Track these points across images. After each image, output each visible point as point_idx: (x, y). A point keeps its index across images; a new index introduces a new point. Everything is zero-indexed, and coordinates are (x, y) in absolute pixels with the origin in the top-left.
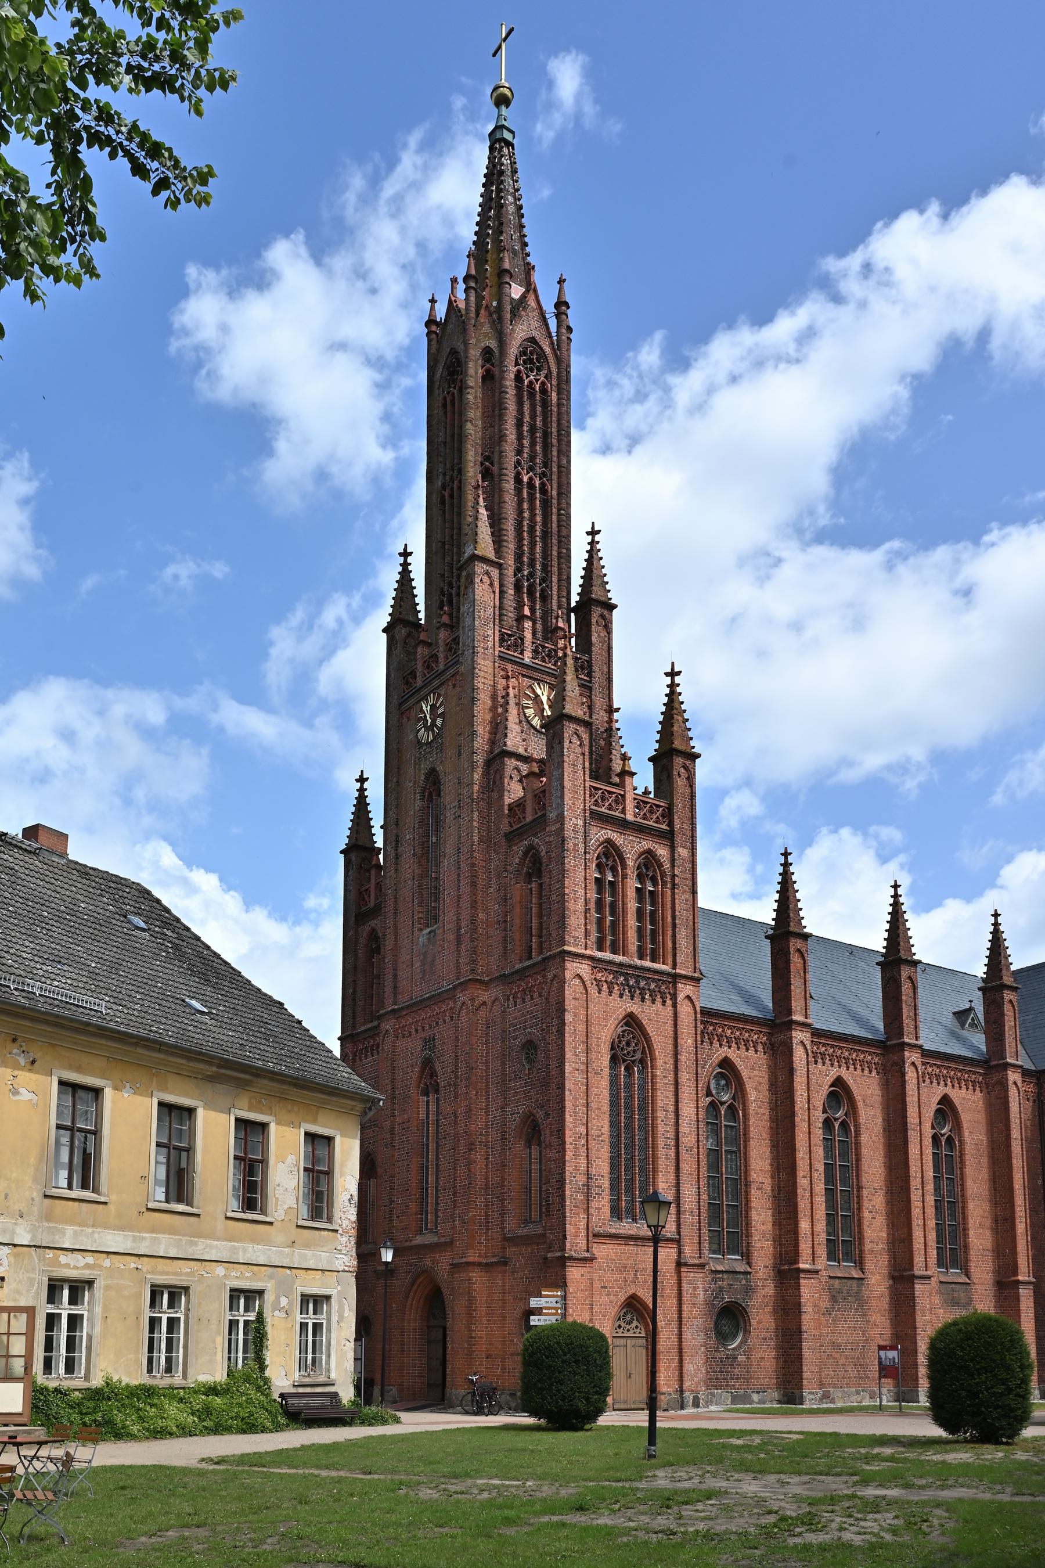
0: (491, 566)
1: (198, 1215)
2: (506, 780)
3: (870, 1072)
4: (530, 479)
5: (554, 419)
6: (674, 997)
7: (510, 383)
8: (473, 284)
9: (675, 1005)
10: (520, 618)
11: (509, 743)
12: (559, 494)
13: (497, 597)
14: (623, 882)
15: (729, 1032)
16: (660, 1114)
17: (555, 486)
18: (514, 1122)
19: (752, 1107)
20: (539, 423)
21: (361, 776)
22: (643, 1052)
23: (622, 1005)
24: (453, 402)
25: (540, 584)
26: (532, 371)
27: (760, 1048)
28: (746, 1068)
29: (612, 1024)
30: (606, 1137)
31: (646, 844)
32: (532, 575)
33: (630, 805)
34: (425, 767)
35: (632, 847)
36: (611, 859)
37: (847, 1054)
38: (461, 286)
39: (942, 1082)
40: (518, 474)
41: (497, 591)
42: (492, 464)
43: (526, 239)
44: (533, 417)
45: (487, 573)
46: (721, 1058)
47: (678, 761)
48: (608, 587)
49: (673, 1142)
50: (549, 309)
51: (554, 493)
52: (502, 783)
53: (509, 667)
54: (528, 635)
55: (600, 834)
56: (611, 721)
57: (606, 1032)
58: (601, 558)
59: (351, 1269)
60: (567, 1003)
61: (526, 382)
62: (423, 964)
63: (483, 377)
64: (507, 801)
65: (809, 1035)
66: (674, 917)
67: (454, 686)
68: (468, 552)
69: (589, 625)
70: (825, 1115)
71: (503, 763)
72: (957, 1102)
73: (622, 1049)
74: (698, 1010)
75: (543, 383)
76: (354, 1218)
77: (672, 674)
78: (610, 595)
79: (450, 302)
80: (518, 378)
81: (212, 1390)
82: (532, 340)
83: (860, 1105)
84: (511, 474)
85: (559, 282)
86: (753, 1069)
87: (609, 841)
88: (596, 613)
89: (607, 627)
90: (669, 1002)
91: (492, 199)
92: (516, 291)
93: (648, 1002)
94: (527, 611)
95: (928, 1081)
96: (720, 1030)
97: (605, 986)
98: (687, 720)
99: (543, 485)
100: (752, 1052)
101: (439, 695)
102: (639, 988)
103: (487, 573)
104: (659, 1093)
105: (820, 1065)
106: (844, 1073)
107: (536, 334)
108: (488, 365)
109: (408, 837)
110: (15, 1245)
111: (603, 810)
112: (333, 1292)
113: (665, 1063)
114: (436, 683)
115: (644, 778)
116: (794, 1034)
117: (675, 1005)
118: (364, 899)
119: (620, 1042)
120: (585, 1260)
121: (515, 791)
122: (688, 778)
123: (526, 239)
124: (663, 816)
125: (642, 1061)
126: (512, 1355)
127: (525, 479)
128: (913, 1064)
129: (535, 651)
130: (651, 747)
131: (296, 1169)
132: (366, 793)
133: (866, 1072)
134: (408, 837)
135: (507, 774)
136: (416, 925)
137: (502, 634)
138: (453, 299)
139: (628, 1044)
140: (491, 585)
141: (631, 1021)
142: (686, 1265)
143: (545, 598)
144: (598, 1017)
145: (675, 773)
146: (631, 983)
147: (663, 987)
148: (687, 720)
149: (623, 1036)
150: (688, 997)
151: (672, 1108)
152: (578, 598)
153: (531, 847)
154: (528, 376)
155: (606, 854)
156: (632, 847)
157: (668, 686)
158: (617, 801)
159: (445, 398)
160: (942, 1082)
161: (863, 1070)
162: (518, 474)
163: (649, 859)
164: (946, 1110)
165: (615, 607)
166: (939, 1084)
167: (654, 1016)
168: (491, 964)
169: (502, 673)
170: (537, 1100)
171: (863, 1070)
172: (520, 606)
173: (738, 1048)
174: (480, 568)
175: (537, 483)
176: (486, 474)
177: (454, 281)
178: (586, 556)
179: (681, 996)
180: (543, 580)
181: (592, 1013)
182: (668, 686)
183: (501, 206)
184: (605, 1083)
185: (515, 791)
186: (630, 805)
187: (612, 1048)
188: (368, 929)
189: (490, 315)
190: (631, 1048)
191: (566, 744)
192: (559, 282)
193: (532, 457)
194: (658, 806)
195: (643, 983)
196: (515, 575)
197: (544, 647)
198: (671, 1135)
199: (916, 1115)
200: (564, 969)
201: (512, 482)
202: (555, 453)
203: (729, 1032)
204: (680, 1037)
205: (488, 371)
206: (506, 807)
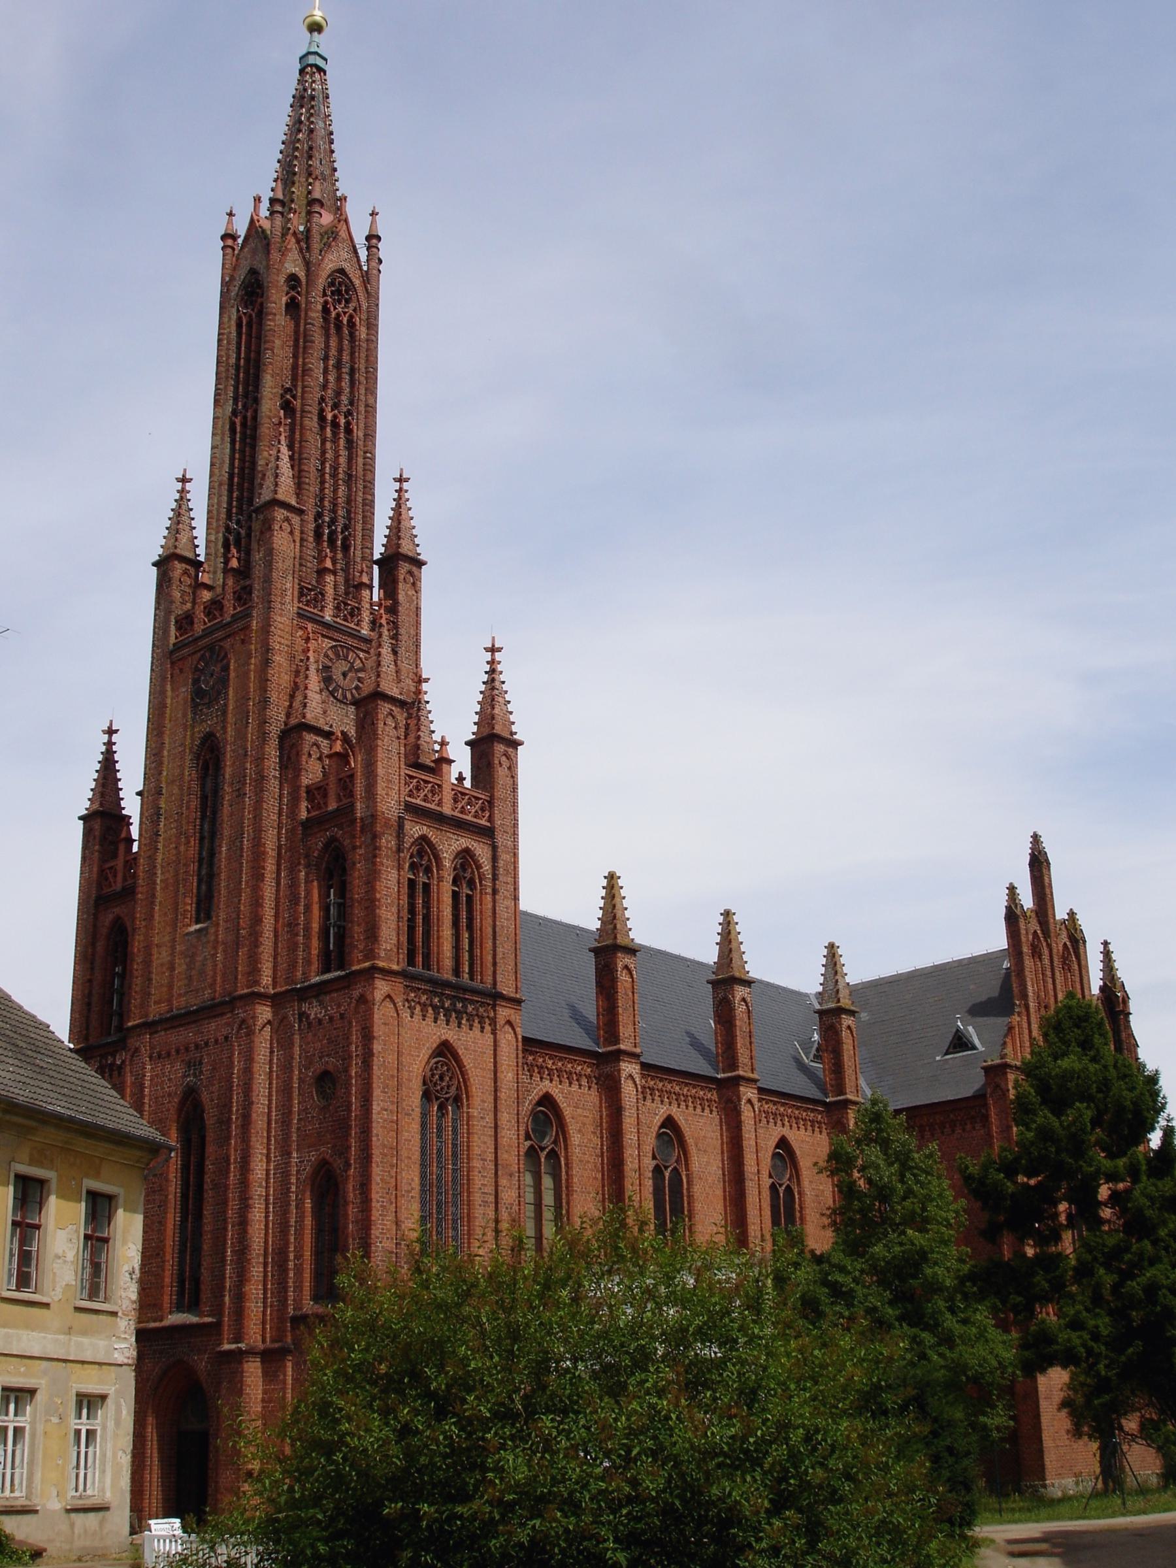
0: (291, 512)
2: (304, 758)
3: (703, 1110)
4: (335, 417)
5: (363, 355)
6: (493, 1022)
7: (316, 315)
8: (279, 208)
10: (321, 572)
11: (308, 716)
12: (366, 435)
13: (298, 547)
14: (438, 885)
15: (550, 1062)
16: (476, 1163)
17: (362, 425)
19: (576, 1152)
20: (346, 357)
21: (110, 728)
22: (458, 1088)
23: (436, 1031)
24: (249, 325)
25: (342, 532)
26: (340, 302)
27: (584, 1082)
28: (569, 1106)
29: (425, 1053)
30: (416, 1193)
31: (464, 842)
32: (333, 521)
33: (448, 796)
35: (450, 845)
36: (426, 858)
37: (677, 1088)
38: (265, 204)
39: (779, 1122)
40: (322, 411)
41: (298, 540)
42: (294, 397)
43: (336, 165)
44: (340, 350)
45: (287, 520)
46: (541, 1093)
47: (500, 748)
48: (417, 541)
49: (492, 1199)
50: (360, 240)
51: (361, 434)
52: (299, 762)
53: (310, 626)
54: (330, 590)
55: (415, 830)
56: (418, 692)
57: (417, 1064)
58: (410, 509)
59: (130, 1362)
60: (376, 1028)
61: (333, 314)
62: (190, 967)
63: (287, 305)
64: (305, 781)
65: (638, 1067)
68: (266, 495)
69: (395, 582)
70: (655, 1162)
71: (301, 738)
72: (795, 1145)
73: (435, 1084)
74: (520, 1037)
75: (351, 317)
76: (134, 1297)
78: (419, 550)
79: (252, 221)
80: (326, 310)
82: (342, 271)
83: (693, 1150)
84: (314, 410)
85: (372, 215)
86: (577, 1107)
87: (424, 838)
88: (404, 568)
89: (415, 585)
90: (488, 1028)
91: (301, 122)
92: (326, 218)
93: (465, 1028)
94: (328, 564)
95: (764, 1121)
96: (541, 1060)
97: (418, 1008)
98: (509, 702)
99: (348, 424)
100: (575, 1087)
102: (455, 1011)
103: (287, 520)
104: (476, 1138)
105: (648, 1103)
106: (675, 1111)
107: (346, 266)
108: (293, 293)
111: (418, 801)
112: (111, 1390)
113: (484, 1101)
115: (462, 763)
116: (623, 1065)
117: (494, 1032)
118: (107, 879)
119: (433, 1075)
121: (312, 772)
122: (509, 768)
123: (336, 165)
124: (483, 809)
125: (457, 1100)
127: (329, 417)
128: (749, 1101)
129: (338, 608)
130: (469, 730)
131: (75, 1236)
132: (114, 748)
133: (699, 1110)
135: (305, 750)
137: (301, 588)
138: (255, 218)
139: (441, 1078)
141: (445, 1050)
143: (346, 547)
144: (410, 1046)
145: (496, 762)
147: (481, 1010)
148: (509, 702)
149: (436, 1068)
150: (509, 1022)
151: (491, 1157)
152: (382, 550)
153: (333, 839)
154: (335, 309)
155: (421, 853)
156: (450, 845)
157: (488, 663)
158: (433, 792)
160: (779, 1122)
161: (695, 1108)
162: (322, 411)
163: (466, 856)
164: (785, 1151)
165: (423, 563)
166: (775, 1123)
167: (471, 1043)
169: (300, 633)
171: (695, 1108)
172: (321, 559)
173: (561, 1082)
174: (280, 514)
175: (342, 421)
176: (287, 407)
177: (257, 200)
178: (393, 504)
179: (501, 1021)
180: (346, 528)
181: (404, 1037)
182: (488, 663)
183: (311, 131)
184: (416, 1127)
185: (312, 772)
186: (448, 796)
187: (424, 1083)
188: (111, 916)
189: (298, 242)
190: (445, 1085)
191: (381, 725)
192: (372, 215)
193: (338, 393)
194: (477, 798)
195: (470, 1008)
196: (316, 520)
197: (346, 604)
198: (490, 1189)
199: (753, 1163)
200: (374, 988)
201: (315, 419)
202: (362, 391)
203: (550, 1062)
204: (499, 1070)
205: (293, 299)
206: (303, 789)
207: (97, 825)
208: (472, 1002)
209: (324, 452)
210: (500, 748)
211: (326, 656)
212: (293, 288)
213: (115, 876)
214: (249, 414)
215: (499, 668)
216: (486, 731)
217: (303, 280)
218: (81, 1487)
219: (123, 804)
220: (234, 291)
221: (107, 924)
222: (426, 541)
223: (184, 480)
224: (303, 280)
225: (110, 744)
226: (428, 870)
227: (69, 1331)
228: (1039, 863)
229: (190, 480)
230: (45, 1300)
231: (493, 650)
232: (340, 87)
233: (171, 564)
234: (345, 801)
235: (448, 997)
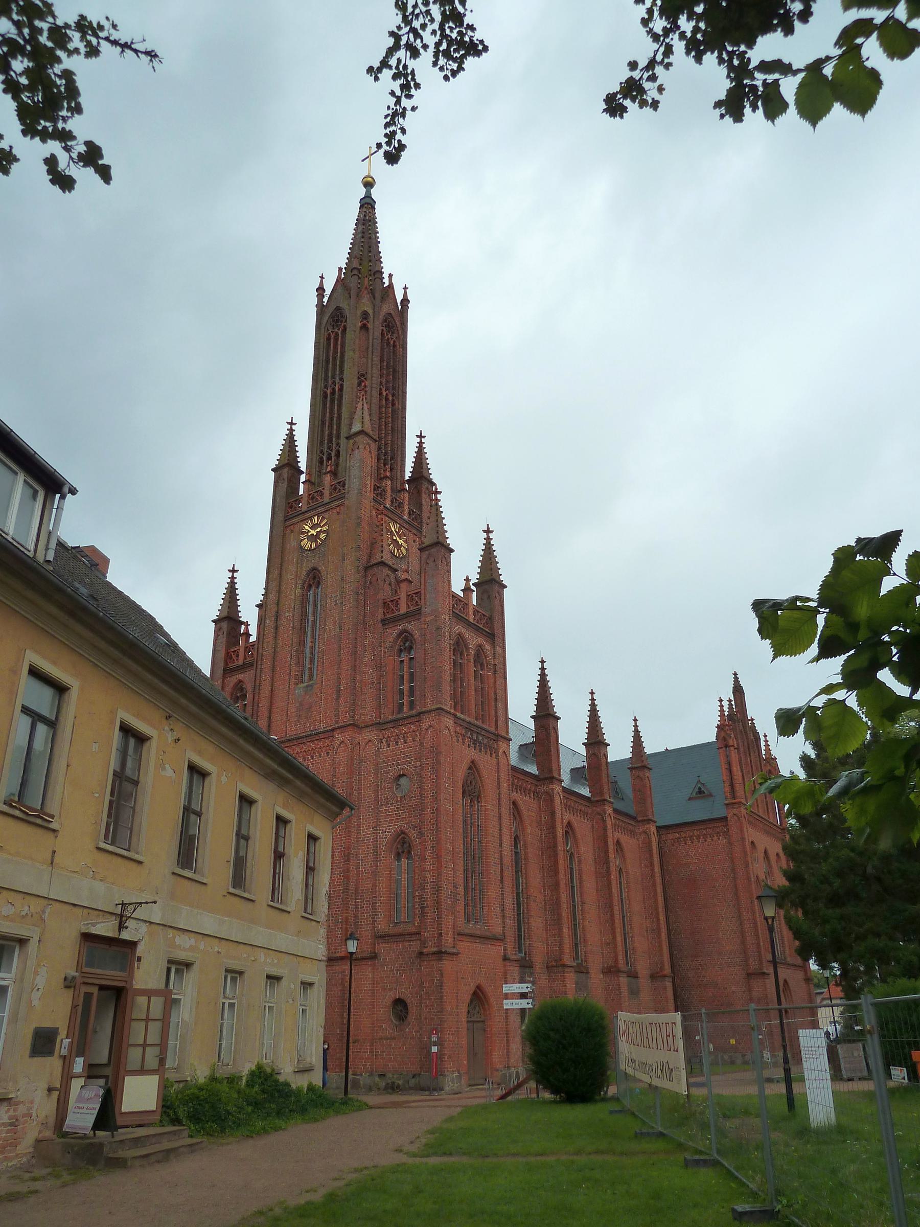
1: (253, 901)
6: (497, 752)
9: (497, 755)
18: (385, 838)
23: (472, 754)
32: (386, 454)
34: (306, 566)
66: (496, 694)
67: (338, 513)
77: (233, 571)
81: (911, 1059)
99: (393, 400)
101: (323, 518)
103: (368, 444)
109: (287, 614)
110: (151, 923)
114: (321, 510)
118: (231, 658)
120: (453, 954)
125: (479, 797)
126: (381, 1039)
127: (384, 394)
134: (287, 614)
136: (293, 680)
140: (370, 452)
141: (473, 766)
142: (509, 959)
146: (475, 737)
153: (405, 631)
159: (329, 334)
167: (485, 761)
168: (367, 714)
170: (410, 822)
177: (340, 269)
207: (224, 625)
209: (380, 413)
210: (496, 587)
212: (366, 318)
213: (238, 656)
214: (329, 392)
215: (492, 542)
216: (488, 578)
217: (371, 314)
218: (76, 1110)
219: (240, 614)
220: (326, 318)
221: (232, 685)
224: (371, 314)
225: (233, 578)
226: (462, 654)
228: (738, 690)
229: (295, 424)
230: (288, 909)
232: (427, 450)
233: (286, 467)
234: (412, 608)
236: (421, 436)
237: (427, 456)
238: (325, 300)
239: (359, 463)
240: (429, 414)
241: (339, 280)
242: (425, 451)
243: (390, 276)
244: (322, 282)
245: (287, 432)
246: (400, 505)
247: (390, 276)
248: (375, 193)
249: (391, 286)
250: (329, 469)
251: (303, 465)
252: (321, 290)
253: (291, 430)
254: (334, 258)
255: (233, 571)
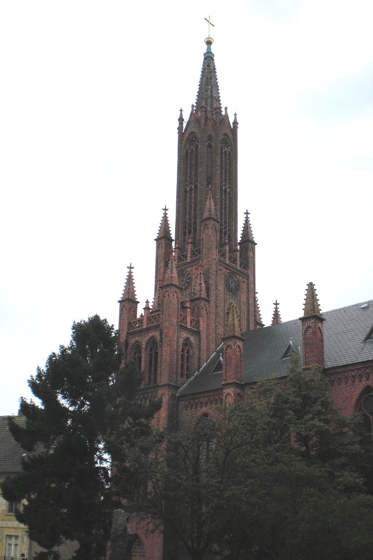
77: (276, 304)
159: (187, 150)
205: (210, 144)
208: (211, 396)
211: (226, 276)
212: (210, 140)
222: (256, 236)
223: (165, 210)
225: (276, 308)
227: (3, 520)
229: (168, 210)
231: (131, 268)
232: (218, 63)
233: (163, 238)
235: (141, 394)
236: (247, 213)
237: (251, 226)
238: (185, 125)
239: (210, 236)
240: (251, 198)
241: (192, 114)
242: (250, 223)
243: (226, 108)
244: (181, 114)
245: (274, 310)
246: (235, 261)
247: (226, 108)
248: (214, 49)
249: (226, 116)
250: (190, 241)
251: (173, 236)
252: (181, 120)
253: (165, 214)
254: (187, 99)
255: (276, 304)
